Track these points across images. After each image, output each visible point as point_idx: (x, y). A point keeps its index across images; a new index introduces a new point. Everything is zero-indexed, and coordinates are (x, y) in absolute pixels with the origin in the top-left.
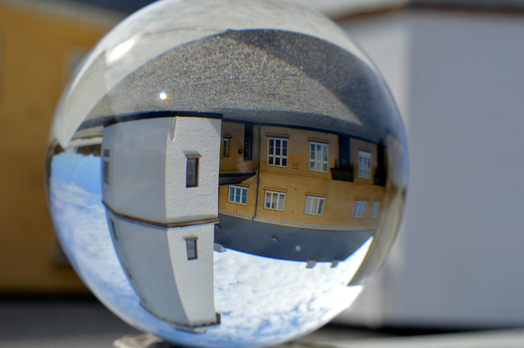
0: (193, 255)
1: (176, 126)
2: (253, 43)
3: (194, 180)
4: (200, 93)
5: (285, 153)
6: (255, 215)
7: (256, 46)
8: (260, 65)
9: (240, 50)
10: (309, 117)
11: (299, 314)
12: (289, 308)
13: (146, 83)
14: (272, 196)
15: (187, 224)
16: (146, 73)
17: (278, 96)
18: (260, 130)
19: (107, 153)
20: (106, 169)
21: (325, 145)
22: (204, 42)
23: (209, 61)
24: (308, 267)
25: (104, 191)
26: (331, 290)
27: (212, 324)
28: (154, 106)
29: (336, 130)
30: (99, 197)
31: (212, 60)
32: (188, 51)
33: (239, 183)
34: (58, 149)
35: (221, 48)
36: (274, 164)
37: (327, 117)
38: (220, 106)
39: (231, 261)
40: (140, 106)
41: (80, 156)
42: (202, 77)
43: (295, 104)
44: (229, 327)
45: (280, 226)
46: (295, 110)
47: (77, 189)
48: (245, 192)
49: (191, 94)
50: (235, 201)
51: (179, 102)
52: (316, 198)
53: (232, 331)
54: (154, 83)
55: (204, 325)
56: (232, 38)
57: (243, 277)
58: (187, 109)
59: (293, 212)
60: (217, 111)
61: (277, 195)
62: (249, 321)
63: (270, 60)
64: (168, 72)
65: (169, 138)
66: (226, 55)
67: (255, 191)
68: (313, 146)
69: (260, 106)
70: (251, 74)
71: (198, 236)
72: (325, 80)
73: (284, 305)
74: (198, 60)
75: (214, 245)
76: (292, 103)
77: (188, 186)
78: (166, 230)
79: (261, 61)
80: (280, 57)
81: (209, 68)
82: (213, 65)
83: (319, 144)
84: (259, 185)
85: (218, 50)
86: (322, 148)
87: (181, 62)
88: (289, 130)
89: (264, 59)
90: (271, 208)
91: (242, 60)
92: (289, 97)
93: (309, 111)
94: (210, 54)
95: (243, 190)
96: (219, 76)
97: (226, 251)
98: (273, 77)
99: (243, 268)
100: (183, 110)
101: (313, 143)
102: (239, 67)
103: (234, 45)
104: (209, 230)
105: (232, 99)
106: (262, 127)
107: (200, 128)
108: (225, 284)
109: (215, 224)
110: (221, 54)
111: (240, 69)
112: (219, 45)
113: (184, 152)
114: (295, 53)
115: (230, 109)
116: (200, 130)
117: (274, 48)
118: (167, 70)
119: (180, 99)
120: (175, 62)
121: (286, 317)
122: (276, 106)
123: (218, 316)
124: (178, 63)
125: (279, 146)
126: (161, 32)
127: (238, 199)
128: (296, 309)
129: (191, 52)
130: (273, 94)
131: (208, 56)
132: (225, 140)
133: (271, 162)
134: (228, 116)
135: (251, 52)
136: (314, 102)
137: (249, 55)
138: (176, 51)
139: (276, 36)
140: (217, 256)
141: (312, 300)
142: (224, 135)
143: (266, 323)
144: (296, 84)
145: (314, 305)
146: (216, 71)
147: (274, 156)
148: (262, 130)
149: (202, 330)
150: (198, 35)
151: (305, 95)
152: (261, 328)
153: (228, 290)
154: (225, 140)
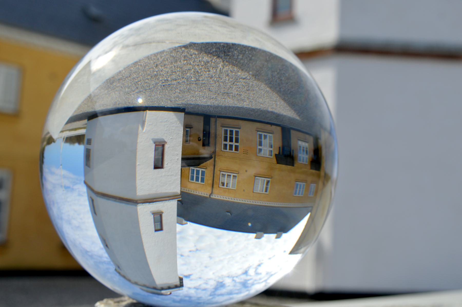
0: (159, 227)
1: (147, 119)
2: (211, 54)
3: (160, 163)
4: (167, 91)
6: (212, 193)
7: (214, 56)
8: (216, 70)
9: (201, 59)
10: (257, 112)
11: (248, 278)
12: (240, 272)
13: (123, 84)
14: (226, 176)
15: (154, 200)
16: (123, 77)
17: (231, 94)
18: (216, 122)
19: (89, 142)
21: (270, 135)
22: (171, 52)
23: (175, 66)
24: (256, 238)
25: (86, 173)
26: (274, 259)
27: (176, 287)
28: (129, 103)
29: (279, 123)
30: (83, 179)
31: (178, 66)
32: (158, 59)
33: (199, 165)
34: (50, 140)
35: (185, 57)
36: (228, 150)
37: (272, 112)
38: (184, 102)
39: (191, 232)
40: (118, 103)
41: (68, 145)
42: (169, 79)
43: (244, 101)
44: (190, 288)
45: (233, 202)
46: (245, 106)
47: (64, 172)
48: (203, 173)
49: (160, 92)
51: (149, 99)
52: (264, 179)
53: (192, 292)
54: (130, 85)
55: (169, 288)
56: (194, 49)
57: (201, 245)
58: (156, 105)
59: (244, 190)
60: (181, 106)
61: (230, 175)
62: (206, 283)
63: (225, 66)
64: (142, 76)
65: (140, 128)
66: (189, 62)
67: (212, 172)
68: (260, 136)
69: (217, 102)
70: (209, 77)
71: (163, 211)
72: (270, 83)
73: (236, 269)
74: (166, 66)
75: (177, 219)
76: (242, 100)
77: (156, 167)
78: (136, 206)
79: (218, 67)
80: (233, 65)
81: (175, 72)
82: (178, 69)
83: (266, 134)
84: (216, 167)
85: (183, 59)
86: (268, 137)
87: (152, 68)
88: (240, 122)
89: (220, 66)
90: (225, 187)
91: (202, 66)
92: (240, 95)
93: (257, 107)
94: (176, 61)
95: (202, 171)
96: (183, 78)
97: (187, 224)
98: (227, 79)
99: (201, 237)
100: (152, 106)
101: (261, 133)
102: (199, 71)
103: (195, 54)
104: (174, 204)
105: (193, 97)
107: (166, 120)
108: (186, 251)
109: (178, 201)
110: (185, 62)
111: (200, 73)
112: (183, 54)
113: (152, 139)
114: (246, 61)
115: (192, 104)
116: (166, 121)
117: (228, 57)
118: (140, 74)
119: (150, 96)
120: (147, 67)
121: (238, 280)
122: (229, 102)
123: (181, 280)
124: (149, 69)
125: (231, 137)
126: (136, 45)
127: (197, 179)
128: (246, 273)
129: (161, 60)
130: (227, 93)
131: (175, 63)
134: (190, 110)
135: (209, 60)
136: (261, 100)
137: (208, 62)
138: (149, 59)
139: (230, 48)
140: (179, 227)
141: (259, 265)
142: (186, 125)
143: (221, 285)
144: (246, 86)
145: (260, 270)
146: (180, 74)
148: (218, 122)
149: (168, 292)
150: (166, 46)
151: (254, 94)
152: (216, 289)
153: (189, 256)
154: (187, 129)
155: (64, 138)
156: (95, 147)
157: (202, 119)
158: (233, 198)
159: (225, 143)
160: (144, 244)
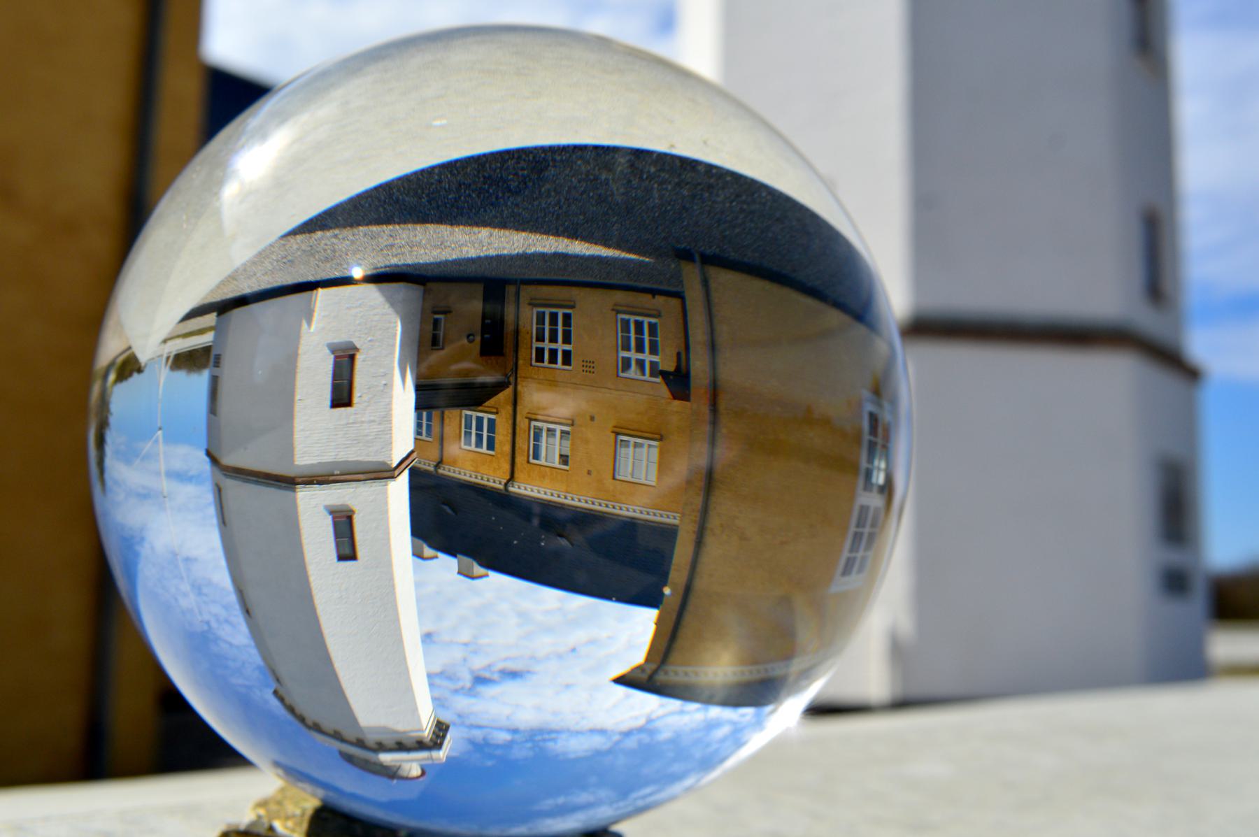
5: (567, 340)
6: (512, 477)
18: (517, 294)
20: (1176, 508)
33: (480, 404)
36: (546, 363)
41: (181, 375)
48: (492, 423)
59: (589, 473)
61: (554, 430)
67: (510, 422)
68: (626, 324)
71: (354, 508)
78: (294, 490)
84: (519, 408)
88: (575, 293)
101: (626, 317)
106: (523, 287)
132: (437, 316)
133: (540, 358)
141: (513, 675)
147: (547, 345)
148: (522, 294)
154: (437, 316)
155: (168, 358)
156: (228, 372)
157: (479, 288)
158: (562, 494)
159: (540, 345)
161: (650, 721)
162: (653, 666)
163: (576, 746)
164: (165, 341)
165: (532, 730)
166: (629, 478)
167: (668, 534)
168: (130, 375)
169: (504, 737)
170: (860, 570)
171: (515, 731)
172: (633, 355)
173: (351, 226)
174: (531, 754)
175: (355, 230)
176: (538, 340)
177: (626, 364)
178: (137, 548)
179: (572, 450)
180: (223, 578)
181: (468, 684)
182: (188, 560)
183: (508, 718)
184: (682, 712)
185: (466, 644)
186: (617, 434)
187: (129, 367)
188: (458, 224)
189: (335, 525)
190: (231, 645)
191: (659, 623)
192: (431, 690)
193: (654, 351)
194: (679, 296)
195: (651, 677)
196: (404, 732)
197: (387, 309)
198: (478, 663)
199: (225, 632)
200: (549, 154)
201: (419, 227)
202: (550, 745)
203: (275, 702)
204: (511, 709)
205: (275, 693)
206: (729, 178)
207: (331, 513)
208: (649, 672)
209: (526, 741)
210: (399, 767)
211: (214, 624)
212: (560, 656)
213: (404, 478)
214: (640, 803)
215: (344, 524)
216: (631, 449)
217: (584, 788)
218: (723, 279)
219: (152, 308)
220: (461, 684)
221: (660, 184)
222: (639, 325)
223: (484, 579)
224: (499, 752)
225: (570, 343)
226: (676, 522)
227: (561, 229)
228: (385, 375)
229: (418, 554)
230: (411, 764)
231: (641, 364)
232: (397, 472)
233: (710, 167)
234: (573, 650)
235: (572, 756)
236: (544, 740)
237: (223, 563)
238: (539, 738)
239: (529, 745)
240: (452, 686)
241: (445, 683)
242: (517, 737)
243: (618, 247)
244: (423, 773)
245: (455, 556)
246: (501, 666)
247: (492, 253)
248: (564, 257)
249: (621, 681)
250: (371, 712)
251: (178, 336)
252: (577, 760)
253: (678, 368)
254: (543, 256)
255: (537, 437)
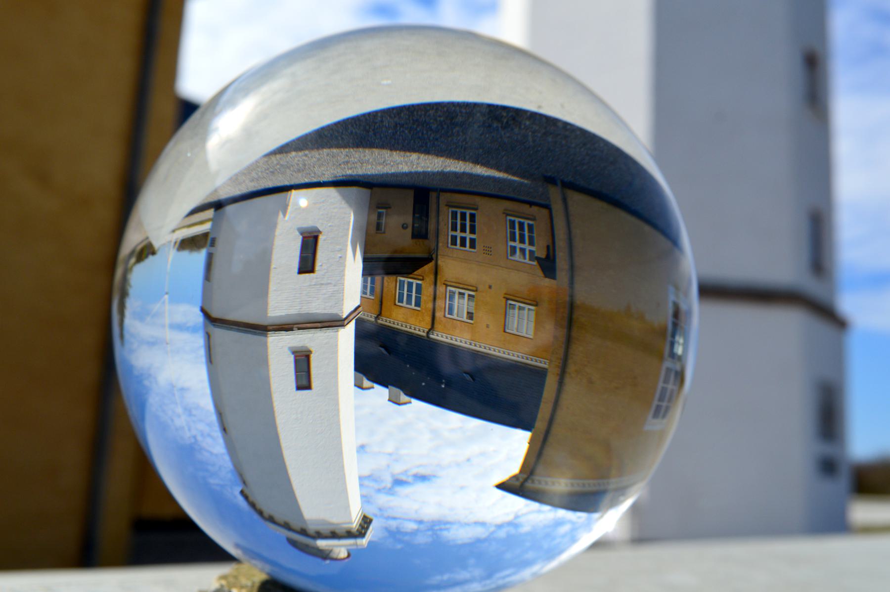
5: (473, 231)
18: (438, 198)
20: (829, 416)
33: (411, 273)
36: (458, 246)
41: (185, 254)
48: (419, 287)
50: (404, 304)
61: (463, 294)
68: (512, 223)
71: (312, 349)
77: (301, 271)
78: (266, 336)
84: (439, 277)
88: (478, 200)
95: (417, 284)
101: (513, 218)
113: (299, 229)
127: (409, 302)
133: (454, 242)
141: (423, 478)
148: (441, 198)
154: (380, 210)
155: (175, 243)
156: (220, 249)
157: (411, 194)
159: (454, 233)
160: (277, 415)
161: (517, 517)
162: (525, 476)
163: (461, 535)
164: (174, 231)
165: (433, 522)
166: (515, 332)
167: (540, 374)
168: (147, 257)
169: (411, 526)
170: (664, 416)
171: (420, 522)
172: (517, 244)
173: (318, 149)
174: (430, 540)
175: (321, 152)
176: (452, 230)
177: (513, 249)
178: (146, 383)
179: (476, 309)
180: (207, 403)
181: (389, 485)
182: (182, 389)
183: (416, 511)
184: (539, 511)
185: (390, 454)
186: (507, 299)
187: (146, 251)
188: (396, 150)
189: (296, 361)
190: (211, 453)
191: (532, 442)
192: (361, 490)
193: (531, 243)
194: (547, 207)
195: (522, 484)
196: (338, 524)
197: (344, 205)
198: (398, 469)
199: (206, 443)
200: (458, 108)
201: (367, 151)
202: (445, 533)
203: (240, 500)
204: (419, 505)
205: (242, 492)
206: (578, 133)
207: (293, 353)
208: (521, 480)
209: (428, 530)
210: (331, 551)
211: (199, 438)
212: (458, 464)
213: (351, 327)
214: (501, 582)
215: (303, 361)
216: (517, 311)
217: (465, 567)
218: (575, 198)
219: (164, 212)
220: (383, 485)
221: (534, 132)
222: (521, 225)
223: (408, 405)
224: (406, 538)
225: (474, 233)
226: (546, 366)
227: (467, 157)
228: (340, 250)
229: (358, 385)
230: (340, 548)
231: (523, 251)
232: (346, 322)
233: (566, 124)
234: (468, 460)
235: (460, 542)
236: (441, 530)
237: (208, 391)
238: (437, 527)
239: (430, 533)
240: (376, 486)
241: (372, 484)
242: (422, 527)
243: (506, 171)
244: (349, 555)
245: (387, 387)
246: (414, 471)
247: (420, 169)
248: (471, 176)
249: (502, 486)
250: (313, 509)
251: (184, 227)
252: (464, 545)
253: (548, 256)
254: (456, 175)
255: (451, 298)
